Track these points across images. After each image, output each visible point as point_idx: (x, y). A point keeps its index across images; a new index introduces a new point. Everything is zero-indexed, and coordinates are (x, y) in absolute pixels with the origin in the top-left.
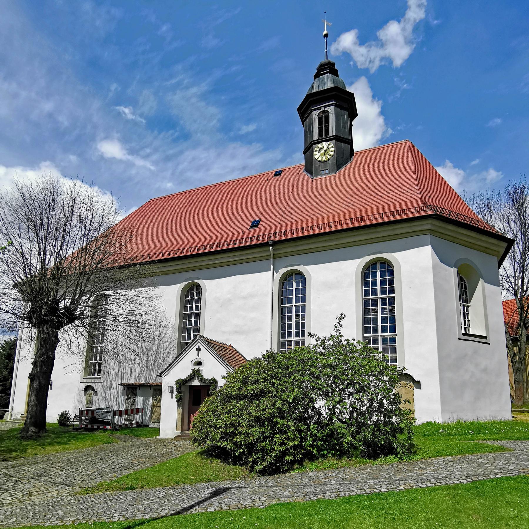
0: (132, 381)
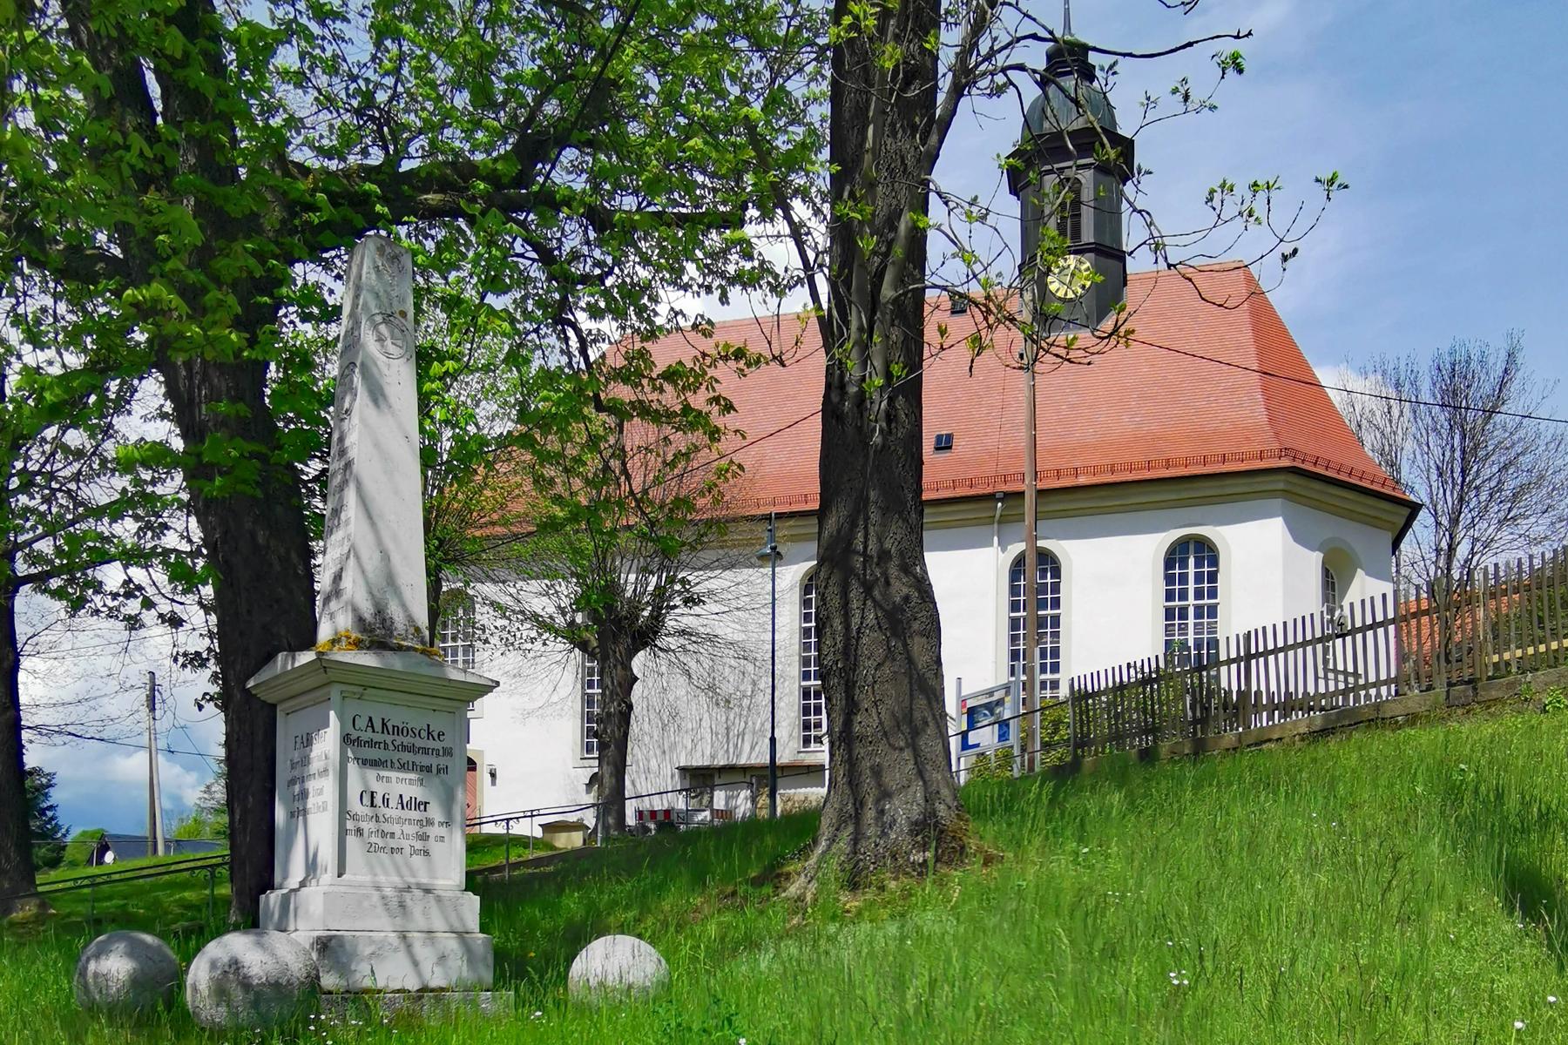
0: (698, 761)
